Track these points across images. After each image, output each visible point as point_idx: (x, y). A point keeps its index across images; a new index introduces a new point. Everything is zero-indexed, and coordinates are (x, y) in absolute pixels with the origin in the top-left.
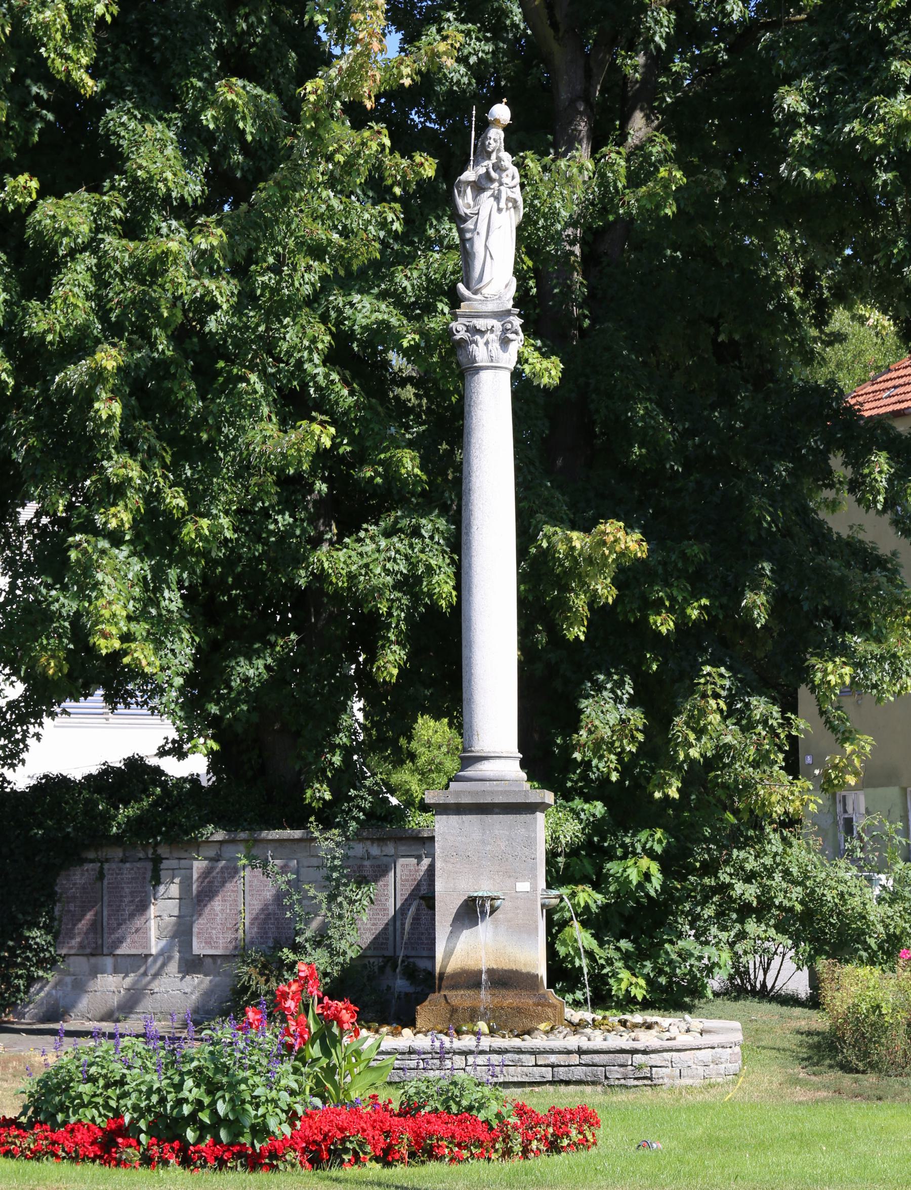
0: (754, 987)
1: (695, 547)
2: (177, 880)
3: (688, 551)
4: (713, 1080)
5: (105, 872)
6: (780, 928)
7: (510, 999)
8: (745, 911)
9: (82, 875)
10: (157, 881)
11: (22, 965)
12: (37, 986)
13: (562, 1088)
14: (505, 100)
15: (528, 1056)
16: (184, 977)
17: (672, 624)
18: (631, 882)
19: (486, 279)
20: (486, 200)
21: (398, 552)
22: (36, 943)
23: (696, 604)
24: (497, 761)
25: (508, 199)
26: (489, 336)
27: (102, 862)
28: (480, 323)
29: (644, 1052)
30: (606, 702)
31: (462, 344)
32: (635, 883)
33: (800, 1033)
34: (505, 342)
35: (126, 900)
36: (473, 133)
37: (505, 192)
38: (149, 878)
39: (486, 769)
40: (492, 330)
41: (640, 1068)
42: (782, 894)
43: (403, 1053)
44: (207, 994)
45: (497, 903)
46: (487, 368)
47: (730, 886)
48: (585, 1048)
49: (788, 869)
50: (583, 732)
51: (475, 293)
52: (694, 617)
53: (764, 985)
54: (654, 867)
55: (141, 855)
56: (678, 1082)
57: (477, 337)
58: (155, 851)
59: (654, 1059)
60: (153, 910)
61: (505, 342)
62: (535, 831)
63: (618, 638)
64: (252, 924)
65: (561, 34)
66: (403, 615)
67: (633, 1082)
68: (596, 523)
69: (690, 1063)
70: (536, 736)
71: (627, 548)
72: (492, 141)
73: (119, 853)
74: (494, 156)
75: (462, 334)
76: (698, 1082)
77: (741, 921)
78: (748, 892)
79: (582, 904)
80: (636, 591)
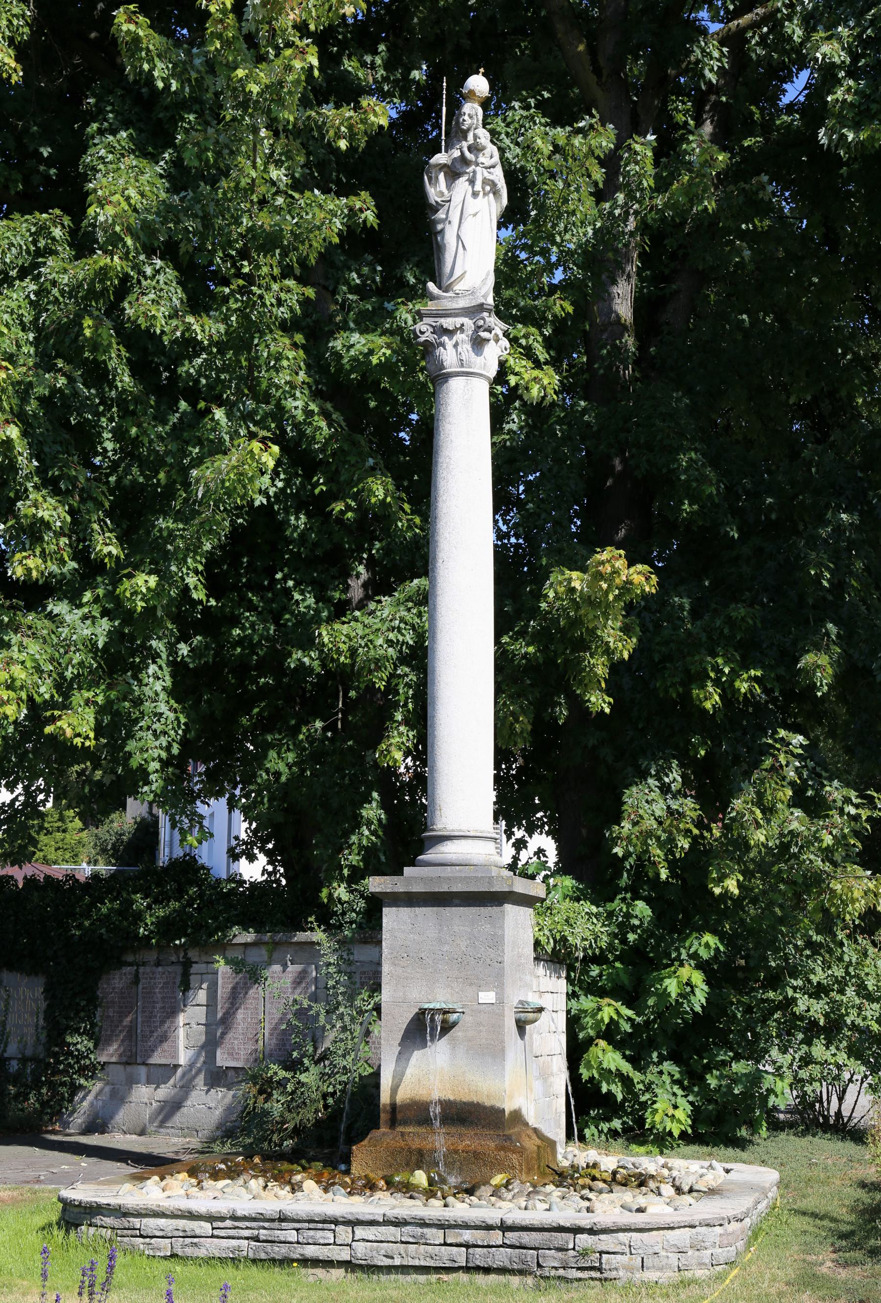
0: (826, 1118)
2: (205, 986)
4: (689, 1274)
5: (140, 976)
6: (854, 1052)
7: (470, 1140)
8: (812, 1030)
9: (121, 979)
10: (186, 986)
11: (65, 1072)
12: (81, 1094)
13: (480, 1279)
15: (434, 1230)
16: (208, 1091)
17: (717, 698)
18: (669, 995)
19: (457, 273)
20: (462, 183)
21: (402, 620)
22: (77, 1050)
23: (745, 676)
24: (463, 842)
25: (485, 182)
26: (459, 336)
27: (138, 965)
28: (448, 323)
29: (591, 1231)
30: (651, 791)
31: (429, 349)
32: (674, 995)
33: (863, 1185)
35: (158, 1006)
36: (444, 109)
38: (178, 983)
39: (449, 851)
40: (461, 328)
41: (584, 1254)
42: (854, 1012)
43: (273, 1220)
44: (229, 1110)
45: (453, 1017)
47: (794, 1000)
48: (509, 1222)
49: (863, 982)
50: (626, 825)
51: (446, 291)
52: (743, 690)
53: (839, 1114)
54: (698, 978)
55: (174, 959)
56: (638, 1276)
57: (445, 338)
58: (186, 954)
59: (606, 1242)
60: (182, 1019)
61: (478, 343)
62: (502, 928)
63: (653, 717)
64: (271, 1034)
65: (604, 80)
66: (411, 692)
67: (574, 1274)
69: (656, 1249)
70: (584, 832)
72: (466, 117)
73: (152, 956)
74: (470, 137)
76: (667, 1276)
77: (808, 1042)
78: (817, 1009)
79: (607, 1021)
80: (679, 664)
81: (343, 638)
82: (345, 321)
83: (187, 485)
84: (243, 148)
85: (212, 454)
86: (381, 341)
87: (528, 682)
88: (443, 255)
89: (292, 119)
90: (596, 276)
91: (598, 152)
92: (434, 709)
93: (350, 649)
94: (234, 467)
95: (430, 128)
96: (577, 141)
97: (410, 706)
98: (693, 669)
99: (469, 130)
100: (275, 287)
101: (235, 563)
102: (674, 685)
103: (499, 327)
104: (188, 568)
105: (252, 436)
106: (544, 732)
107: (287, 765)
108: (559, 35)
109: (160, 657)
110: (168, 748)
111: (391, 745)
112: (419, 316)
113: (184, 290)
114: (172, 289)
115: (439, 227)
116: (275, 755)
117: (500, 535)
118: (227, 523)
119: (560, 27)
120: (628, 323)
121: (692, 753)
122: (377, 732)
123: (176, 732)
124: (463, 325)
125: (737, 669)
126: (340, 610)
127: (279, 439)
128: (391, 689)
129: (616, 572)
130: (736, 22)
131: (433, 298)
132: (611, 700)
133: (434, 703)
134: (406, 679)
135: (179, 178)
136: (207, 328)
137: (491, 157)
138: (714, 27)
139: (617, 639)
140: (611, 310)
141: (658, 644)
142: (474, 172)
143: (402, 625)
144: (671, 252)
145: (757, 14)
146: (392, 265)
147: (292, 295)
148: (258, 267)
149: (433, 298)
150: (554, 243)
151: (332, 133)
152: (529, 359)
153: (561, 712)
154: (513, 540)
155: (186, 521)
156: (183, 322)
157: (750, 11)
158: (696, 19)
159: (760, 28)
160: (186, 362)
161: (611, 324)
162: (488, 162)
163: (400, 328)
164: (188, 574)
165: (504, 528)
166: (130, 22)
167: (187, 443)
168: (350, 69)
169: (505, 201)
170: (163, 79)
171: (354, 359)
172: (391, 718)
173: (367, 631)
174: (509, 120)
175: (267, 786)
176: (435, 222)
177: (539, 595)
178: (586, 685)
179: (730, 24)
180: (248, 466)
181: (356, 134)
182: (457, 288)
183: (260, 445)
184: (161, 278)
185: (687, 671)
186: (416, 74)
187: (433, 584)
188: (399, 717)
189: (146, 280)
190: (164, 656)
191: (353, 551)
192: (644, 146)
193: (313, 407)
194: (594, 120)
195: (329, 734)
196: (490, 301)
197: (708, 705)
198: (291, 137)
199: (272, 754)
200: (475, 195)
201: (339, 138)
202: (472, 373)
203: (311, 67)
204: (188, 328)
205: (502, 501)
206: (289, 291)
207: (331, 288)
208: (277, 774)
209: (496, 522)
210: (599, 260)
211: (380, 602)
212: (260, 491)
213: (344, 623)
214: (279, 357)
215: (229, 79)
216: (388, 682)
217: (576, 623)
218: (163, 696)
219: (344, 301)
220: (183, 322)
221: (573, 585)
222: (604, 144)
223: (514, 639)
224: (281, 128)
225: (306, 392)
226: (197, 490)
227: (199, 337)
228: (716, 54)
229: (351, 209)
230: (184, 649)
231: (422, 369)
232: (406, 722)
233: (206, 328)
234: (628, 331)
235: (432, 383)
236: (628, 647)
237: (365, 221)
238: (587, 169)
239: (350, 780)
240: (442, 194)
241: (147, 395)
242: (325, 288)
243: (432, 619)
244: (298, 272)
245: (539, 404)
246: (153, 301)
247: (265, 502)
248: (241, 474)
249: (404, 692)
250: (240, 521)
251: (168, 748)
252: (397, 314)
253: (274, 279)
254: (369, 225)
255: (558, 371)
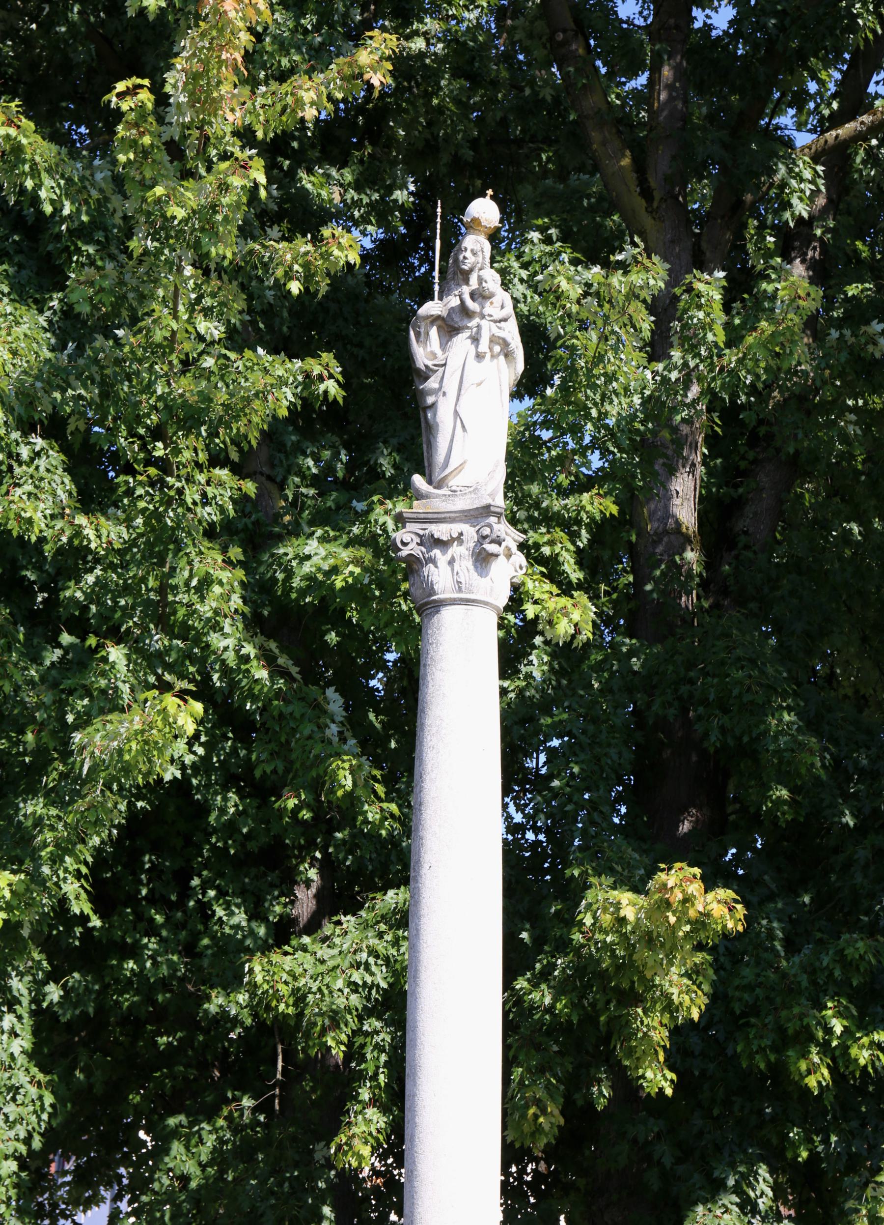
1: (860, 944)
3: (849, 951)
14: (490, 192)
17: (825, 1072)
19: (453, 464)
20: (461, 341)
21: (373, 953)
23: (865, 1040)
25: (493, 340)
26: (455, 550)
28: (441, 531)
34: (483, 559)
37: (488, 329)
46: (453, 602)
51: (438, 487)
52: (862, 1062)
57: (436, 552)
61: (483, 559)
65: (655, 205)
66: (383, 1058)
68: (651, 872)
71: (708, 915)
72: (468, 254)
75: (413, 549)
81: (285, 976)
82: (297, 523)
83: (66, 754)
84: (161, 292)
85: (102, 712)
86: (345, 555)
87: (555, 1048)
88: (435, 438)
89: (229, 255)
90: (647, 463)
91: (644, 294)
92: (415, 1084)
93: (295, 991)
94: (136, 733)
95: (416, 263)
96: (617, 280)
97: (382, 1079)
98: (791, 1028)
99: (471, 270)
100: (201, 478)
101: (134, 865)
102: (762, 1050)
103: (511, 537)
104: (66, 870)
105: (164, 687)
106: (580, 1119)
107: (200, 1164)
108: (595, 146)
109: (20, 1003)
110: (28, 1141)
111: (353, 1136)
112: (400, 520)
113: (74, 480)
114: (56, 477)
115: (430, 400)
116: (182, 1150)
117: (512, 828)
118: (123, 807)
119: (595, 136)
120: (690, 532)
121: (789, 1155)
122: (333, 1117)
123: (39, 1117)
124: (461, 534)
125: (853, 1028)
126: (283, 933)
127: (203, 691)
128: (354, 1053)
129: (687, 900)
130: (834, 133)
131: (419, 496)
132: (674, 1077)
133: (415, 1074)
134: (377, 1039)
135: (70, 328)
136: (104, 532)
137: (502, 307)
138: (803, 139)
139: (683, 990)
140: (667, 514)
141: (737, 988)
142: (479, 327)
143: (371, 960)
144: (751, 440)
145: (862, 123)
146: (360, 447)
147: (225, 488)
148: (177, 451)
149: (419, 496)
150: (588, 416)
151: (280, 272)
152: (552, 581)
153: (601, 1092)
154: (530, 836)
155: (64, 805)
156: (72, 524)
157: (853, 118)
158: (778, 127)
159: (866, 140)
160: (72, 583)
161: (666, 532)
162: (498, 314)
163: (375, 536)
164: (65, 879)
165: (518, 818)
166: (9, 125)
167: (71, 692)
168: (309, 186)
169: (520, 367)
170: (52, 202)
171: (310, 578)
172: (356, 1098)
173: (321, 968)
174: (526, 259)
175: (169, 1197)
176: (424, 394)
177: (569, 920)
178: (638, 1059)
179: (827, 135)
180: (154, 729)
181: (314, 275)
182: (453, 483)
183: (177, 700)
184: (42, 463)
185: (781, 1030)
186: (400, 196)
187: (415, 897)
188: (365, 1095)
189: (20, 465)
190: (25, 1001)
191: (301, 848)
192: (710, 286)
193: (249, 649)
194: (638, 250)
195: (262, 1118)
196: (499, 501)
197: (812, 1082)
198: (225, 278)
199: (177, 1147)
200: (479, 357)
201: (291, 278)
202: (474, 601)
203: (256, 185)
204: (78, 532)
205: (514, 777)
206: (221, 484)
207: (278, 479)
208: (184, 1179)
209: (505, 806)
210: (649, 447)
211: (339, 923)
212: (172, 761)
213: (286, 954)
214: (206, 582)
215: (144, 200)
216: (350, 1045)
217: (624, 967)
218: (21, 1060)
219: (296, 495)
220: (72, 524)
221: (622, 913)
222: (652, 282)
223: (535, 984)
224: (213, 266)
225: (241, 626)
226: (83, 762)
227: (93, 546)
228: (807, 174)
229: (307, 375)
230: (54, 993)
231: (406, 594)
232: (374, 1102)
233: (102, 532)
234: (690, 542)
235: (418, 613)
236: (698, 1001)
237: (326, 392)
238: (631, 317)
239: (291, 1187)
240: (434, 355)
241: (15, 624)
242: (270, 478)
243: (414, 949)
244: (234, 456)
245: (568, 644)
246: (30, 494)
247: (179, 776)
248: (146, 742)
249: (375, 1061)
250: (140, 804)
251: (28, 1141)
252: (372, 517)
253: (199, 466)
254: (331, 399)
255: (594, 598)
